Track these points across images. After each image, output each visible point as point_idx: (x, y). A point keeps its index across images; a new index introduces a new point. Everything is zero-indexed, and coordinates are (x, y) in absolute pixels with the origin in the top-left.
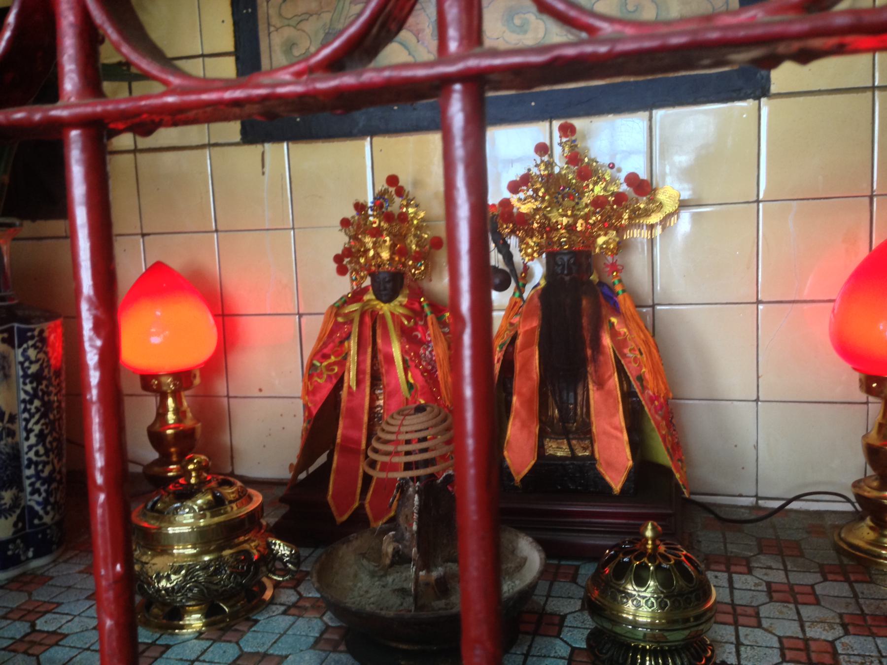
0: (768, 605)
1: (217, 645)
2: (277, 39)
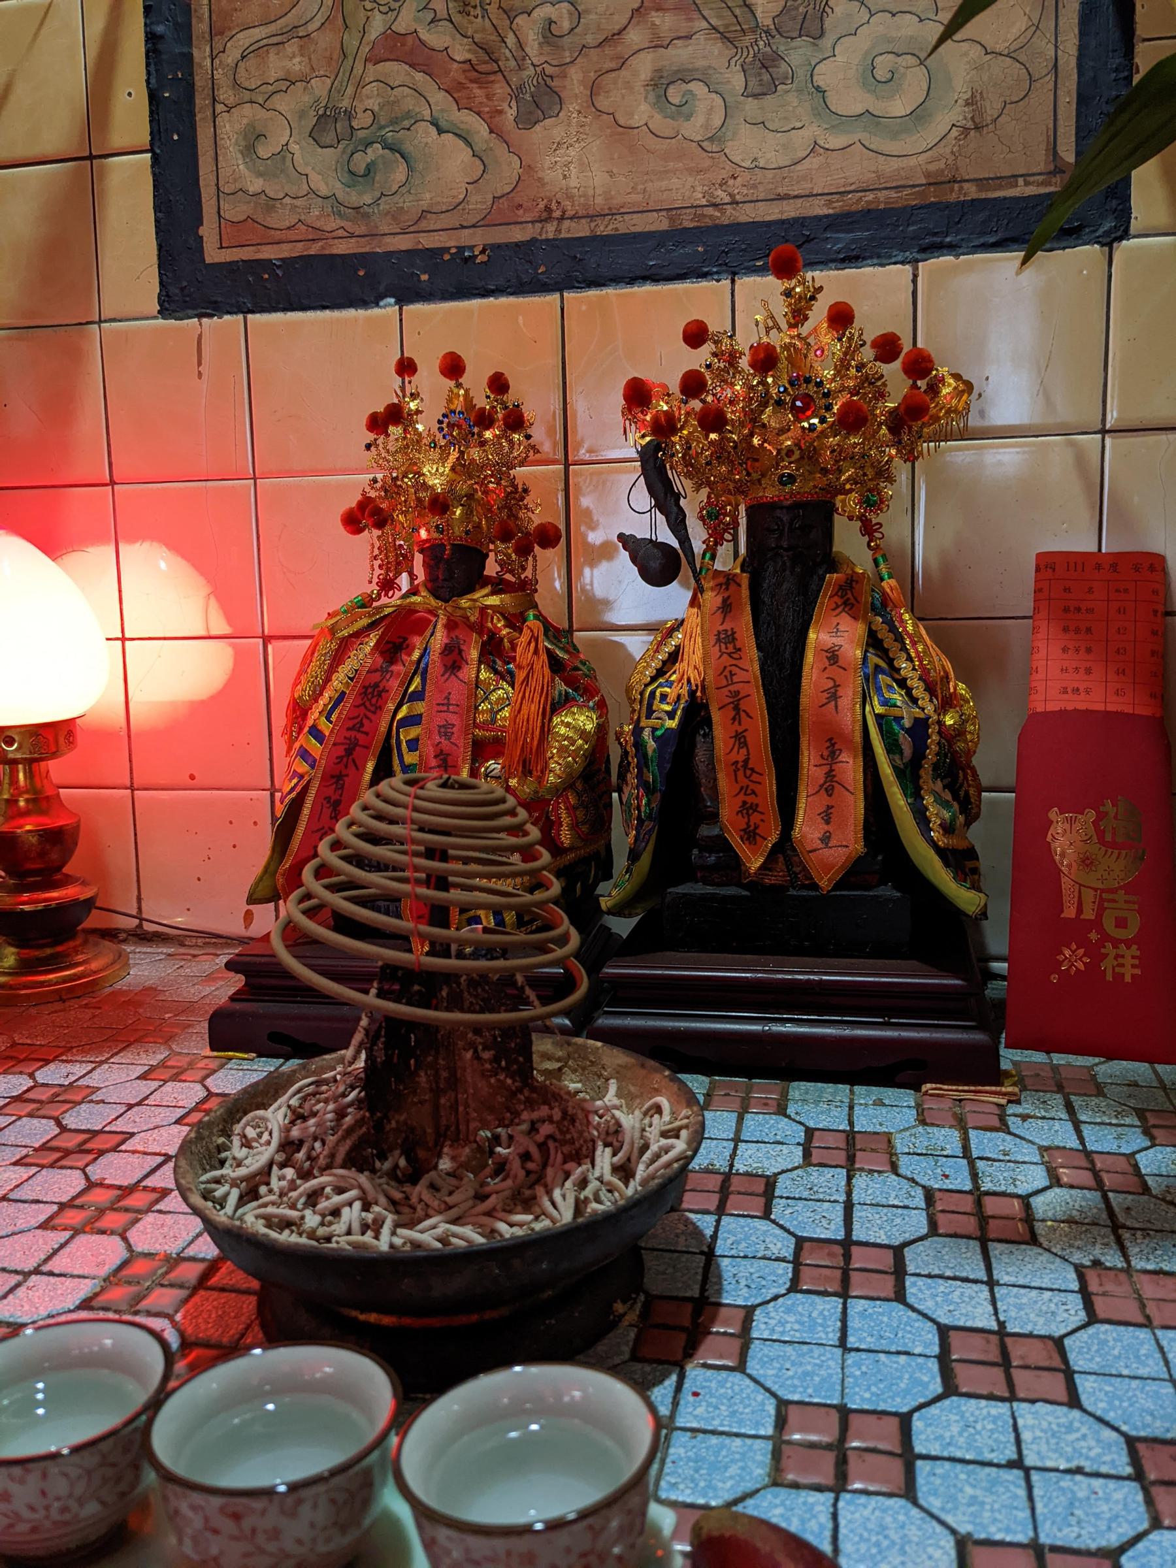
1: (82, 1239)
2: (231, 127)
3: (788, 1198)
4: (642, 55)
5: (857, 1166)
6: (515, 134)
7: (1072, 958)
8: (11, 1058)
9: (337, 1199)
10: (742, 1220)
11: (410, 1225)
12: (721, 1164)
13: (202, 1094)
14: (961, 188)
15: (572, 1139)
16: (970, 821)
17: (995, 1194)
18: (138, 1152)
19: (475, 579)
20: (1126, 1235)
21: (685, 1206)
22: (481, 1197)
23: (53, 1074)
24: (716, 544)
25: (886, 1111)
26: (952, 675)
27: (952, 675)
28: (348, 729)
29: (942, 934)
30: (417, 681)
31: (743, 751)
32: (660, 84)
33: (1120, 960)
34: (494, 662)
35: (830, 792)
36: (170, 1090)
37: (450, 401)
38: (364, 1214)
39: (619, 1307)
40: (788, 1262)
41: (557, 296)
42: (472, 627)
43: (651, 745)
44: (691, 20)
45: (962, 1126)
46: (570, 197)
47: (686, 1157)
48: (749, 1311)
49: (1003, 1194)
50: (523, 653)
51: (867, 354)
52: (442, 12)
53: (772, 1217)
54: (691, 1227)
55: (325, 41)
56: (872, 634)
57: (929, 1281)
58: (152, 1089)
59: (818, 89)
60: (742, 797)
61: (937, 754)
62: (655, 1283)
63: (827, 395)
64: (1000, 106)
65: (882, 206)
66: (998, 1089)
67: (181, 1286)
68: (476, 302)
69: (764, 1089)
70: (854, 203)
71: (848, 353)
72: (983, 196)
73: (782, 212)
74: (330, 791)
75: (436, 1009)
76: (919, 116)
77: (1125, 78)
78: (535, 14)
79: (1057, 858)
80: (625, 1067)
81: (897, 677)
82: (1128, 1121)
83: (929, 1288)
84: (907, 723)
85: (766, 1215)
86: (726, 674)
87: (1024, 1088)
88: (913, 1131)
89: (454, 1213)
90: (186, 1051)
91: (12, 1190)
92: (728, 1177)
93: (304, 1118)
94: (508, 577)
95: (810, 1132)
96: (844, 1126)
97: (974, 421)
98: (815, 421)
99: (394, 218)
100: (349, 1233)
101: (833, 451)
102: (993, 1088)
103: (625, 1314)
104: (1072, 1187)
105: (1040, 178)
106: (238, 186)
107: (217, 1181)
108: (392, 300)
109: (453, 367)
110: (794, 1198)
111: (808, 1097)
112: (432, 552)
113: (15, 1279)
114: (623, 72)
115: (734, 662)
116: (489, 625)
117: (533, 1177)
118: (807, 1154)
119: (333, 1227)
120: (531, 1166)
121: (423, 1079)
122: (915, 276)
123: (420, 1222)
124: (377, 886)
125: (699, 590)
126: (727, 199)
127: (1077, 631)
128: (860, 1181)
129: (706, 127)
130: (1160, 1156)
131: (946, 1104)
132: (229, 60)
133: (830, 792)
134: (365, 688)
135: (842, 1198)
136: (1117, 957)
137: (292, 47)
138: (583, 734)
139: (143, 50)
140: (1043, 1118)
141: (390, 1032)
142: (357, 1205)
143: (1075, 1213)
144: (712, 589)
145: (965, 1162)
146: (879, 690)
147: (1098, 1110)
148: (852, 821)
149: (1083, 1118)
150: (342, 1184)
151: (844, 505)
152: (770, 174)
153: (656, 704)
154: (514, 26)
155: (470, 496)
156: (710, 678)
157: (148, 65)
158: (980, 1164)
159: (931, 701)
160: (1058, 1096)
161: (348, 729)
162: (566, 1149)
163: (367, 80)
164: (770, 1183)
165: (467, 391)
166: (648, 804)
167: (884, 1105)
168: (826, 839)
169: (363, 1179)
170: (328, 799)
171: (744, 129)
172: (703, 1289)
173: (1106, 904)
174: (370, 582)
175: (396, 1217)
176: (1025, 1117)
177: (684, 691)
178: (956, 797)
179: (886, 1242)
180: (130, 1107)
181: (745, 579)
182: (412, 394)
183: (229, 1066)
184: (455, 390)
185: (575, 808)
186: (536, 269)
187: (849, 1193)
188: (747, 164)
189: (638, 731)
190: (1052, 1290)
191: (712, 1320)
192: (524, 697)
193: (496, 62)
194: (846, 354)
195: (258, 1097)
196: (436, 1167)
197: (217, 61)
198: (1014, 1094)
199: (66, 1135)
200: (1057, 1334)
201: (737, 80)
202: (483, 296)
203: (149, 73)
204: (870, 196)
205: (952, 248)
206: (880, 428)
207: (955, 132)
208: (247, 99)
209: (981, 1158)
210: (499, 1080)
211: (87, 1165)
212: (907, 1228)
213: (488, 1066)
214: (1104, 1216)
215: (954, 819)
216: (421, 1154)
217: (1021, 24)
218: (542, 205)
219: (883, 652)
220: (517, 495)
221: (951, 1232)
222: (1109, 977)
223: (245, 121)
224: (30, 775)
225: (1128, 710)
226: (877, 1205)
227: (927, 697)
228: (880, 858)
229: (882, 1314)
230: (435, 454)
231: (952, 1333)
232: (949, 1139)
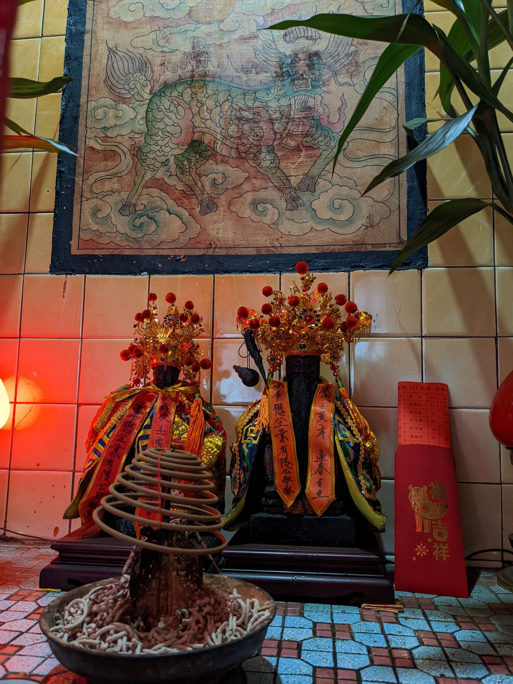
0: (370, 668)
2: (87, 206)
3: (308, 650)
4: (249, 193)
5: (337, 637)
6: (199, 217)
7: (421, 550)
9: (115, 636)
10: (288, 659)
11: (149, 648)
12: (277, 636)
13: (36, 606)
14: (366, 247)
16: (377, 489)
17: (397, 648)
18: (7, 630)
19: (175, 381)
20: (453, 664)
21: (262, 654)
22: (179, 638)
24: (273, 371)
25: (346, 615)
26: (368, 427)
27: (368, 427)
28: (117, 440)
29: (366, 535)
31: (285, 454)
32: (255, 204)
33: (441, 551)
34: (181, 414)
35: (321, 473)
36: (21, 604)
37: (169, 311)
38: (128, 643)
40: (310, 676)
41: (212, 275)
42: (172, 400)
43: (246, 451)
44: (267, 183)
45: (380, 621)
46: (219, 240)
47: (270, 619)
49: (401, 649)
51: (333, 302)
52: (174, 173)
53: (302, 658)
54: (266, 662)
55: (128, 179)
56: (337, 408)
58: (12, 604)
59: (313, 209)
60: (284, 474)
61: (364, 458)
63: (318, 316)
64: (379, 219)
65: (336, 251)
66: (394, 606)
68: (180, 276)
69: (293, 606)
70: (325, 249)
72: (374, 250)
73: (299, 251)
74: (106, 467)
76: (350, 221)
77: (424, 213)
78: (209, 176)
79: (413, 506)
81: (347, 426)
82: (449, 620)
84: (352, 444)
85: (299, 657)
86: (278, 422)
87: (405, 607)
88: (360, 623)
89: (168, 642)
90: (27, 588)
92: (280, 642)
95: (315, 624)
96: (329, 621)
97: (373, 331)
98: (314, 325)
99: (149, 243)
102: (392, 606)
104: (429, 646)
105: (395, 245)
106: (88, 227)
107: (57, 631)
108: (146, 273)
109: (171, 298)
110: (310, 650)
112: (158, 370)
114: (241, 199)
115: (281, 417)
116: (180, 399)
117: (201, 630)
118: (314, 633)
119: (114, 648)
120: (200, 625)
121: (154, 584)
122: (349, 277)
123: (153, 646)
126: (279, 245)
127: (416, 413)
128: (338, 644)
129: (272, 219)
130: (464, 634)
132: (90, 182)
133: (321, 473)
134: (126, 423)
135: (331, 650)
136: (439, 549)
137: (115, 180)
138: (217, 446)
139: (56, 176)
140: (414, 618)
141: (146, 557)
142: (125, 638)
143: (431, 656)
144: (272, 388)
145: (383, 636)
146: (340, 430)
147: (436, 615)
148: (330, 485)
149: (431, 619)
150: (118, 629)
152: (295, 238)
154: (201, 180)
155: (175, 347)
156: (271, 423)
157: (57, 181)
158: (389, 637)
159: (361, 436)
160: (419, 610)
161: (117, 440)
162: (216, 618)
163: (143, 194)
164: (299, 645)
165: (176, 307)
167: (346, 613)
168: (319, 493)
169: (127, 627)
170: (105, 471)
171: (286, 222)
173: (434, 526)
174: (130, 380)
175: (142, 644)
176: (406, 618)
177: (261, 429)
178: (371, 478)
179: (352, 668)
181: (286, 384)
182: (154, 307)
183: (48, 595)
184: (171, 307)
186: (204, 265)
187: (334, 648)
188: (286, 233)
189: (240, 445)
192: (193, 429)
193: (193, 191)
194: (325, 302)
196: (157, 626)
197: (84, 182)
198: (401, 608)
201: (284, 205)
202: (183, 274)
203: (57, 184)
204: (332, 247)
205: (363, 267)
206: (338, 329)
207: (363, 227)
208: (95, 196)
209: (390, 634)
210: (187, 585)
212: (361, 662)
213: (183, 579)
214: (444, 657)
215: (371, 487)
216: (150, 620)
217: (387, 192)
218: (208, 243)
220: (195, 348)
222: (437, 558)
223: (94, 204)
225: (437, 445)
226: (347, 653)
227: (359, 435)
228: (341, 502)
230: (163, 330)
232: (375, 627)
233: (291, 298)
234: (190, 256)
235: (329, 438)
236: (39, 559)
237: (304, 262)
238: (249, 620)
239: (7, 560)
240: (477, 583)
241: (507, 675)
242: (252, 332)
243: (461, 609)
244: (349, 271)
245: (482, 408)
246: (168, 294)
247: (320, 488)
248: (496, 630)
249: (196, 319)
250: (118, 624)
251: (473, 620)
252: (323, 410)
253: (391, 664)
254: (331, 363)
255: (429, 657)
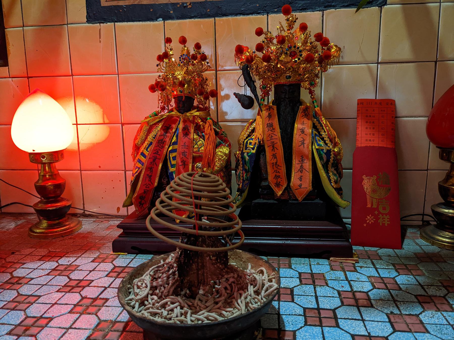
0: (342, 308)
1: (83, 316)
3: (298, 295)
7: (370, 219)
8: (50, 256)
11: (196, 313)
13: (113, 267)
15: (240, 284)
20: (398, 303)
22: (216, 303)
23: (64, 261)
24: (265, 96)
25: (321, 266)
28: (154, 153)
29: (331, 211)
30: (175, 138)
31: (275, 160)
33: (384, 219)
35: (301, 172)
37: (182, 51)
38: (181, 310)
39: (256, 333)
41: (213, 19)
42: (191, 122)
43: (247, 158)
48: (294, 332)
50: (207, 129)
51: (313, 39)
56: (314, 124)
57: (345, 320)
60: (275, 173)
62: (265, 325)
63: (300, 51)
67: (118, 331)
68: (188, 20)
69: (283, 260)
71: (306, 38)
75: (198, 246)
80: (250, 258)
82: (390, 267)
83: (346, 323)
84: (325, 151)
85: (293, 301)
89: (209, 309)
91: (58, 300)
93: (156, 279)
94: (201, 106)
95: (300, 274)
98: (296, 59)
100: (177, 317)
101: (303, 69)
103: (257, 335)
104: (379, 289)
108: (161, 19)
109: (183, 41)
111: (297, 262)
112: (178, 99)
113: (64, 331)
118: (301, 281)
119: (172, 315)
120: (228, 291)
121: (194, 266)
123: (198, 312)
124: (173, 205)
125: (260, 110)
128: (318, 289)
131: (338, 264)
133: (301, 172)
135: (314, 295)
136: (383, 218)
138: (225, 154)
140: (366, 267)
141: (184, 251)
142: (179, 307)
144: (265, 110)
145: (347, 282)
147: (381, 264)
149: (378, 267)
150: (173, 301)
151: (304, 85)
153: (248, 145)
155: (190, 81)
158: (352, 282)
162: (239, 286)
165: (187, 48)
166: (246, 175)
167: (320, 264)
169: (179, 299)
172: (279, 326)
176: (361, 267)
177: (257, 141)
178: (337, 173)
180: (91, 271)
181: (275, 107)
183: (119, 257)
185: (223, 177)
187: (316, 293)
189: (242, 153)
190: (381, 322)
191: (284, 335)
194: (305, 39)
195: (138, 272)
199: (72, 281)
200: (386, 336)
202: (190, 18)
205: (334, 7)
209: (352, 281)
211: (80, 291)
213: (214, 262)
214: (391, 297)
215: (337, 179)
216: (194, 289)
219: (317, 130)
220: (204, 81)
221: (348, 304)
224: (49, 168)
225: (385, 146)
227: (330, 143)
229: (334, 332)
231: (355, 337)
233: (278, 37)
234: (195, 3)
235: (308, 147)
236: (110, 229)
237: (287, 5)
238: (262, 289)
239: (89, 231)
240: (406, 238)
241: (436, 311)
242: (248, 67)
243: (397, 258)
244: (323, 11)
245: (420, 117)
246: (180, 38)
247: (301, 182)
248: (424, 275)
249: (204, 58)
250: (172, 297)
251: (406, 267)
252: (304, 126)
253: (356, 305)
254: (309, 89)
255: (381, 298)
